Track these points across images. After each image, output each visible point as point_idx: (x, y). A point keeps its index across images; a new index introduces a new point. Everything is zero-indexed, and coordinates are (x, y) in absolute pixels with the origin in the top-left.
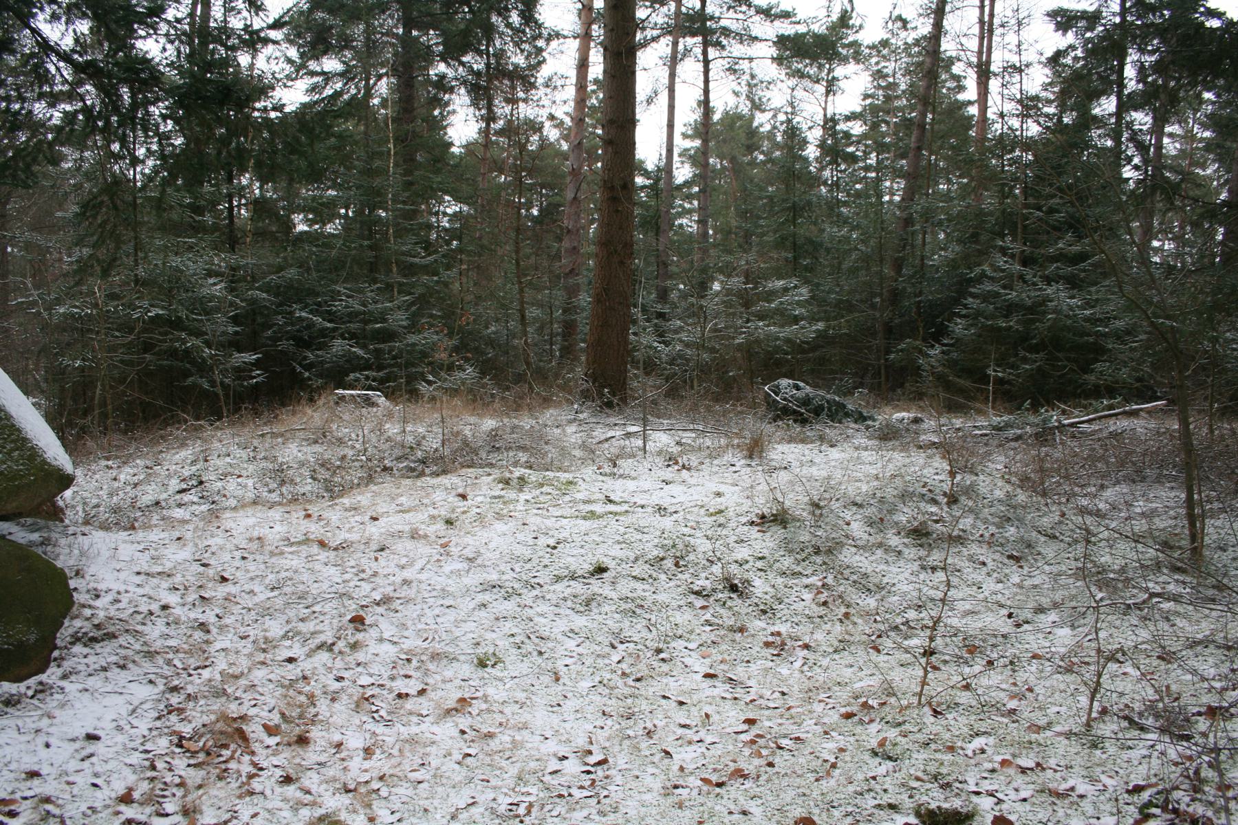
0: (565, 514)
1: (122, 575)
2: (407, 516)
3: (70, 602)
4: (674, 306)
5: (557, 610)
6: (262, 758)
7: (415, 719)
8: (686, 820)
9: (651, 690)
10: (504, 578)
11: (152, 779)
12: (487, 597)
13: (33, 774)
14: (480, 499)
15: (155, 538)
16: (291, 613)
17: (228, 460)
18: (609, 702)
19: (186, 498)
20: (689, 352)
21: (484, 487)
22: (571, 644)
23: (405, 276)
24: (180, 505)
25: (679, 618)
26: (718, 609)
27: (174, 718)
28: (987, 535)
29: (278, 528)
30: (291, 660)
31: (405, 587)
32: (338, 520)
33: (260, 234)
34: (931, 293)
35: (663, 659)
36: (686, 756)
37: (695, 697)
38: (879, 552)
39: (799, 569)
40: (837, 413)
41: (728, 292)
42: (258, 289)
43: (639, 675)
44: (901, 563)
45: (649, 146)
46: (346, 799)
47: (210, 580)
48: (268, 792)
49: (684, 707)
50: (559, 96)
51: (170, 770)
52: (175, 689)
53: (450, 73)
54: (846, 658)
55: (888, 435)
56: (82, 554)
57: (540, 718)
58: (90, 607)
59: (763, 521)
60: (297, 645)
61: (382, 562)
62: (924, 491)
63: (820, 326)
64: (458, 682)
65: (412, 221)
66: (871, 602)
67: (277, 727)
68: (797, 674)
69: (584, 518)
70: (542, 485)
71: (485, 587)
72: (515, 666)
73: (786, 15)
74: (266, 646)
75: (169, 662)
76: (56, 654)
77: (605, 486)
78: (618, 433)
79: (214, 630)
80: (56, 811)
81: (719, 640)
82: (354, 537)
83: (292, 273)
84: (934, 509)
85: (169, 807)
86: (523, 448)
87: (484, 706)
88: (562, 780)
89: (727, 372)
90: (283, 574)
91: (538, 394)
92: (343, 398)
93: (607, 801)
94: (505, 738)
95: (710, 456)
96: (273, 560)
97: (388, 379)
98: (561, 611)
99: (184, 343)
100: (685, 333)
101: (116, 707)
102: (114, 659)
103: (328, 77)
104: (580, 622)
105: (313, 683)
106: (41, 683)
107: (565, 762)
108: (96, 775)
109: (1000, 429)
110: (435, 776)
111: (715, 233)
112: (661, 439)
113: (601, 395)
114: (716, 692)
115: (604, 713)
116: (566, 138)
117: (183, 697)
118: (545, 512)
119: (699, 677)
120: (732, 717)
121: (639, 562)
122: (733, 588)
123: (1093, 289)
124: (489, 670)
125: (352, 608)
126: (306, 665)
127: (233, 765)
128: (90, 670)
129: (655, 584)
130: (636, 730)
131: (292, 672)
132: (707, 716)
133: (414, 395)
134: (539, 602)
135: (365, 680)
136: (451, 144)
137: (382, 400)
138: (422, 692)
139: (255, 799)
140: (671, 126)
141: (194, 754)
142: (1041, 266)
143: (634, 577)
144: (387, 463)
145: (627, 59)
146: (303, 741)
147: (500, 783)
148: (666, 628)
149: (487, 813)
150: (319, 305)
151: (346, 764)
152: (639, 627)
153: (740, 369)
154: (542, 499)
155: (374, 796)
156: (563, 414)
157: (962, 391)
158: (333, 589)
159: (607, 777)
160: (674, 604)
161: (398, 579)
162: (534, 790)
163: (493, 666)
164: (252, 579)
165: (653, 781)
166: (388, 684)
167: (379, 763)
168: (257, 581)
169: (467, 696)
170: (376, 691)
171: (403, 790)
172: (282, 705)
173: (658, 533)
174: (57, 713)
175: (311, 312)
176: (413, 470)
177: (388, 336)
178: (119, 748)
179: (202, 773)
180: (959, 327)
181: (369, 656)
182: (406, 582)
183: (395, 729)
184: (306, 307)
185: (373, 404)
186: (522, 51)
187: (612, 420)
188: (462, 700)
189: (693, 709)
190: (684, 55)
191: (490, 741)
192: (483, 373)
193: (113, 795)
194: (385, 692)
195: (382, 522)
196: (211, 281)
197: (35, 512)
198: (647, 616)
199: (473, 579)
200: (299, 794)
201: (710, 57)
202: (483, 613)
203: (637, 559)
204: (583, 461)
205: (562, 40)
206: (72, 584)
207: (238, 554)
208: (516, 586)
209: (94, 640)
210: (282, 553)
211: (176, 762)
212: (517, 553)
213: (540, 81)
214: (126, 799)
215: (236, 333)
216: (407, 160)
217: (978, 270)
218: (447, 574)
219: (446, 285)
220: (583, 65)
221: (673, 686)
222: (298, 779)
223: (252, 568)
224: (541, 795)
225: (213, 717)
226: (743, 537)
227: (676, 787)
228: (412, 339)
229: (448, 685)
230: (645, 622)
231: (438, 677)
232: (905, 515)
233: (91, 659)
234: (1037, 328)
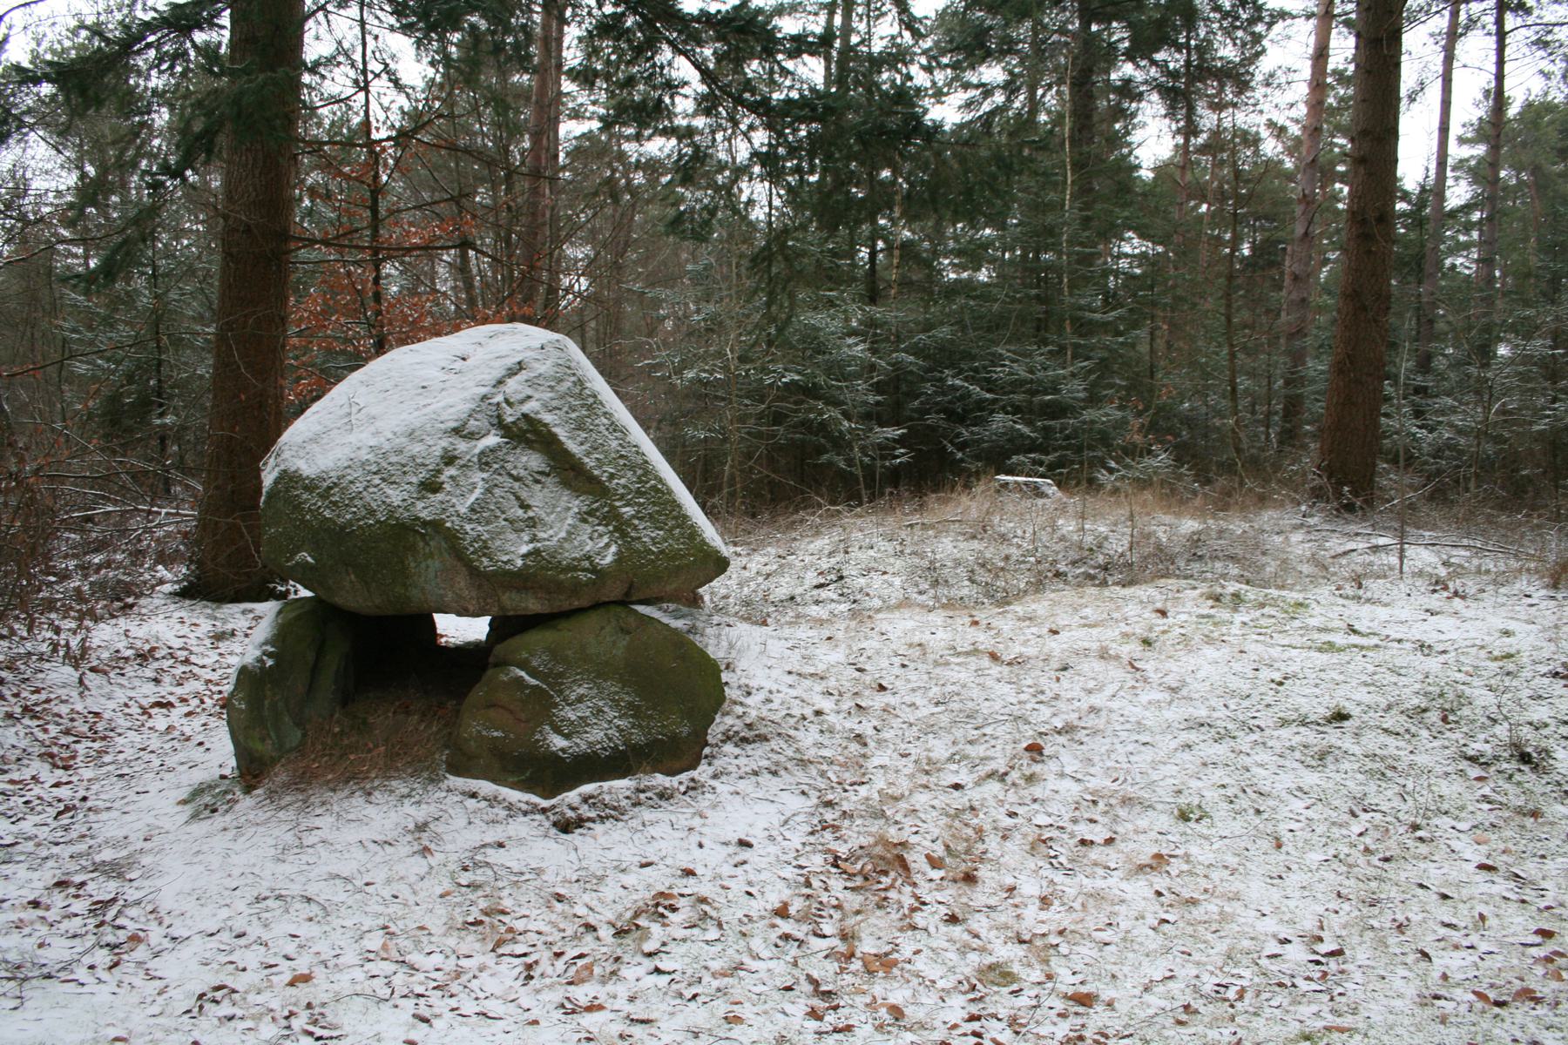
0: (1294, 643)
1: (775, 673)
2: (1094, 631)
3: (721, 698)
4: (1442, 377)
5: (1281, 762)
6: (924, 891)
7: (1100, 871)
8: (1452, 1039)
9: (1403, 875)
10: (1215, 715)
11: (808, 896)
12: (1192, 736)
13: (689, 873)
14: (1183, 617)
15: (804, 636)
16: (959, 733)
17: (871, 552)
18: (1347, 882)
19: (824, 594)
20: (1462, 441)
21: (1189, 604)
22: (1298, 805)
23: (1081, 336)
24: (817, 602)
25: (1444, 788)
26: (1501, 783)
27: (828, 835)
29: (940, 634)
30: (957, 787)
31: (1092, 715)
32: (1010, 629)
33: (905, 283)
35: (1421, 839)
36: (1453, 962)
37: (1464, 891)
41: (1527, 360)
42: (904, 350)
43: (1388, 854)
45: (1413, 163)
46: (1020, 951)
47: (866, 688)
48: (932, 929)
49: (1449, 902)
50: (1290, 96)
51: (826, 889)
53: (1139, 76)
56: (731, 646)
57: (1256, 889)
58: (741, 704)
60: (964, 771)
61: (1065, 683)
64: (1153, 835)
65: (1087, 268)
67: (941, 859)
69: (1320, 650)
70: (1262, 606)
71: (1191, 724)
72: (1225, 823)
74: (930, 767)
75: (823, 774)
76: (707, 751)
77: (1347, 613)
78: (1361, 545)
79: (872, 744)
80: (714, 914)
81: (1502, 823)
82: (1030, 651)
83: (944, 332)
85: (827, 928)
86: (1232, 558)
87: (1185, 867)
88: (1284, 967)
89: (1517, 470)
90: (950, 688)
91: (1250, 490)
93: (1343, 999)
94: (1211, 908)
95: (1495, 582)
96: (938, 670)
97: (1060, 463)
98: (1287, 763)
99: (821, 414)
100: (1457, 419)
101: (768, 816)
102: (765, 763)
103: (987, 91)
104: (1310, 779)
105: (981, 816)
106: (693, 780)
107: (1287, 946)
108: (750, 883)
110: (1124, 939)
111: (1504, 275)
112: (1422, 557)
114: (1495, 889)
115: (1339, 895)
116: (1290, 151)
117: (838, 814)
118: (1268, 639)
119: (1471, 867)
120: (1520, 924)
121: (1393, 712)
122: (1525, 758)
124: (1192, 824)
125: (1028, 735)
126: (973, 795)
127: (892, 894)
128: (741, 772)
129: (1414, 741)
130: (1383, 921)
131: (958, 800)
132: (1482, 917)
133: (1093, 485)
134: (1259, 749)
135: (1042, 820)
136: (1138, 167)
137: (1052, 490)
138: (1109, 841)
139: (919, 935)
140: (1444, 129)
141: (851, 876)
143: (1386, 730)
144: (1062, 567)
145: (1389, 46)
146: (970, 879)
147: (1204, 959)
148: (1426, 799)
149: (1188, 991)
150: (976, 370)
151: (1019, 911)
152: (1389, 793)
153: (1538, 466)
154: (1263, 622)
155: (1052, 951)
156: (1289, 518)
158: (1006, 711)
159: (1342, 972)
160: (1439, 770)
161: (1084, 706)
162: (1247, 973)
163: (1197, 821)
164: (913, 690)
165: (1405, 985)
166: (1070, 827)
167: (1056, 916)
169: (1164, 852)
170: (1054, 833)
171: (1087, 950)
172: (946, 835)
173: (1420, 677)
174: (709, 813)
175: (966, 379)
176: (1092, 578)
177: (1058, 410)
178: (772, 859)
179: (860, 898)
181: (1048, 792)
182: (1093, 710)
183: (1077, 880)
184: (959, 373)
185: (1042, 495)
186: (1234, 40)
187: (1353, 528)
188: (1158, 856)
189: (1461, 906)
190: (1467, 28)
191: (1192, 908)
192: (1179, 461)
193: (769, 907)
194: (1065, 836)
195: (1064, 635)
196: (850, 341)
197: (674, 598)
198: (1401, 781)
199: (1175, 714)
200: (966, 936)
201: (1508, 27)
202: (1187, 756)
203: (1389, 707)
204: (1313, 579)
205: (1289, 21)
206: (725, 677)
207: (897, 661)
208: (1230, 727)
209: (745, 740)
210: (947, 664)
211: (831, 882)
213: (1259, 77)
214: (782, 912)
215: (878, 403)
216: (1084, 190)
218: (1143, 706)
219: (1133, 346)
220: (1321, 55)
221: (1434, 875)
222: (965, 920)
223: (914, 678)
224: (1256, 980)
225: (871, 840)
226: (1541, 692)
227: (1437, 997)
228: (1089, 414)
229: (1142, 837)
230: (1397, 789)
231: (1130, 826)
233: (742, 761)
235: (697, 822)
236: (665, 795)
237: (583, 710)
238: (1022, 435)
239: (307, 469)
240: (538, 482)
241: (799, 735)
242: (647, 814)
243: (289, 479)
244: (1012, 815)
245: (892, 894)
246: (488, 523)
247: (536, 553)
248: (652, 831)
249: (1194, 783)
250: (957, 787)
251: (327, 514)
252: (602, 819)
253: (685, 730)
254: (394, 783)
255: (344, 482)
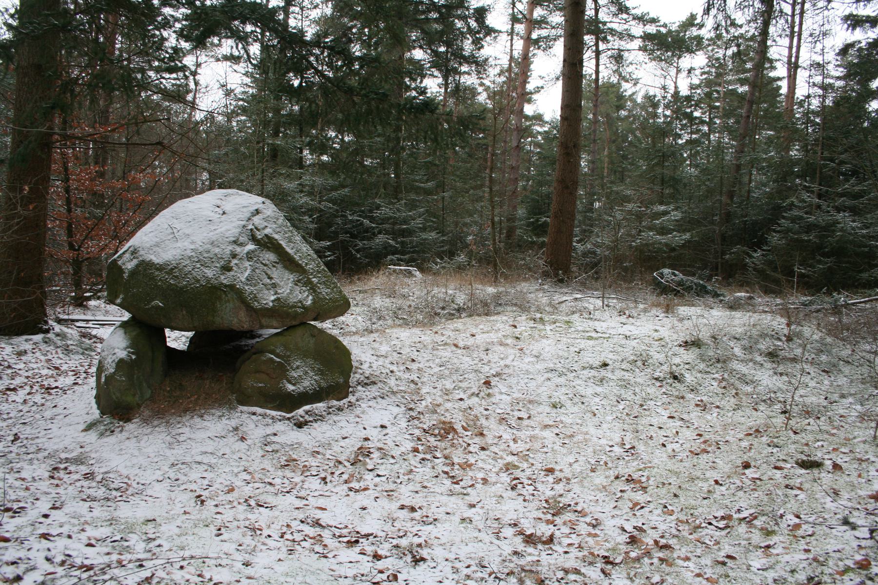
12: (550, 375)
16: (455, 378)
22: (597, 400)
25: (649, 390)
28: (810, 359)
30: (461, 399)
34: (754, 216)
38: (751, 364)
39: (708, 370)
40: (702, 292)
44: (763, 370)
46: (515, 458)
52: (411, 409)
54: (740, 413)
55: (733, 306)
59: (686, 344)
60: (462, 393)
62: (773, 333)
63: (687, 236)
66: (749, 389)
68: (715, 419)
70: (555, 323)
72: (570, 408)
73: (653, 21)
74: (447, 392)
75: (403, 397)
76: (351, 389)
84: (779, 343)
85: (438, 455)
92: (395, 271)
94: (580, 437)
100: (602, 239)
104: (599, 390)
109: (806, 305)
113: (556, 275)
119: (665, 418)
122: (675, 378)
123: (868, 216)
131: (464, 405)
138: (529, 418)
142: (833, 199)
150: (363, 212)
157: (777, 282)
166: (511, 413)
168: (431, 362)
170: (507, 416)
175: (360, 216)
177: (409, 233)
180: (775, 239)
182: (506, 366)
199: (540, 366)
201: (601, 48)
202: (549, 383)
203: (623, 360)
209: (366, 384)
212: (560, 354)
217: (788, 201)
221: (655, 421)
232: (763, 345)
234: (829, 241)
235: (358, 419)
236: (340, 409)
237: (300, 372)
238: (391, 246)
239: (156, 260)
240: (274, 266)
241: (388, 381)
242: (335, 418)
243: (145, 266)
244: (486, 410)
245: (455, 441)
246: (255, 286)
247: (278, 299)
248: (340, 424)
249: (555, 393)
250: (461, 399)
251: (172, 282)
252: (316, 421)
253: (342, 380)
254: (213, 411)
255: (181, 267)
